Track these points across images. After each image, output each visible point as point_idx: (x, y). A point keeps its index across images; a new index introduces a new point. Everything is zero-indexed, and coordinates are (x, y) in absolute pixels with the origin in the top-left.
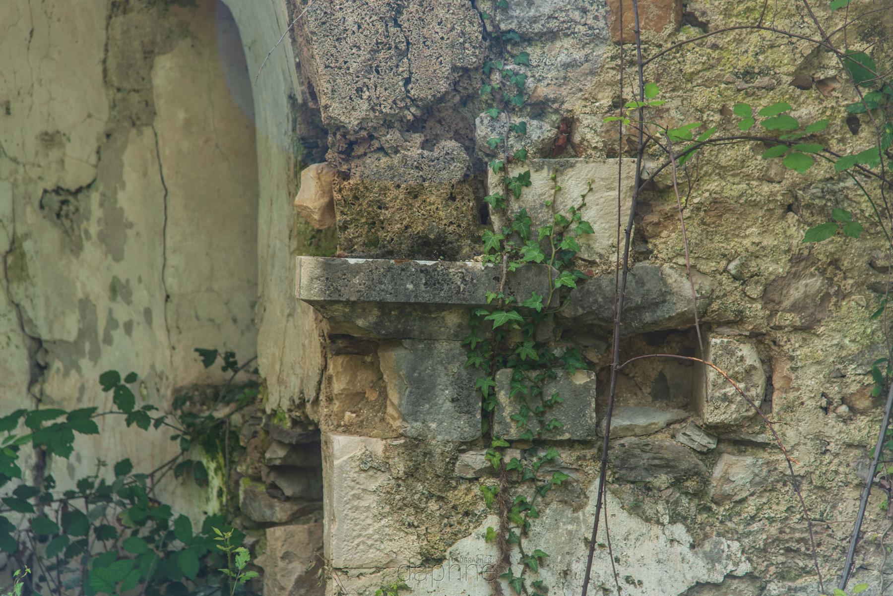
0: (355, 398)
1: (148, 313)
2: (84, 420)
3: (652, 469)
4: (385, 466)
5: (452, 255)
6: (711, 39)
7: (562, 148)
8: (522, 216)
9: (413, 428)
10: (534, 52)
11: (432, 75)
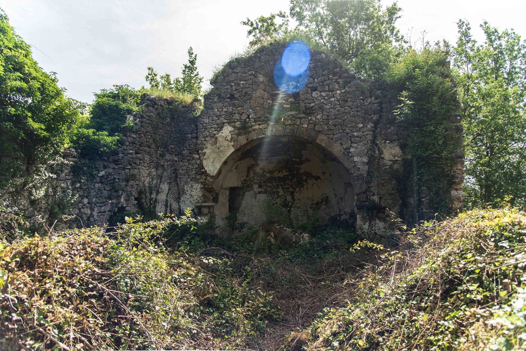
2: (342, 215)
7: (374, 195)
11: (364, 190)
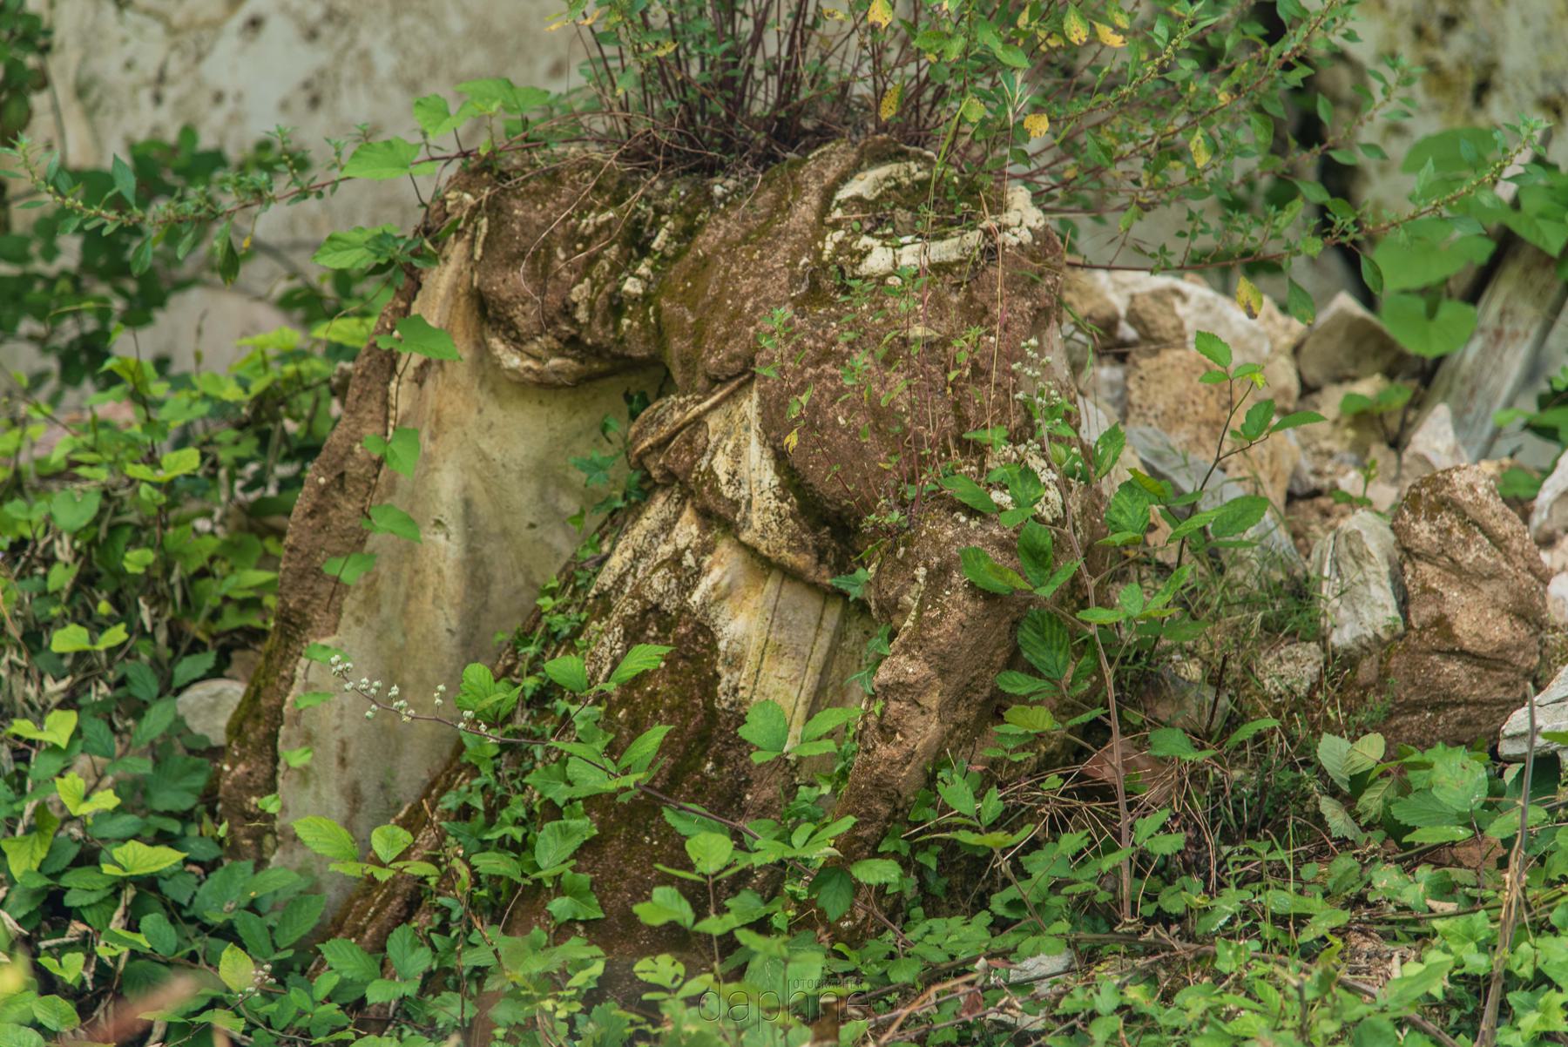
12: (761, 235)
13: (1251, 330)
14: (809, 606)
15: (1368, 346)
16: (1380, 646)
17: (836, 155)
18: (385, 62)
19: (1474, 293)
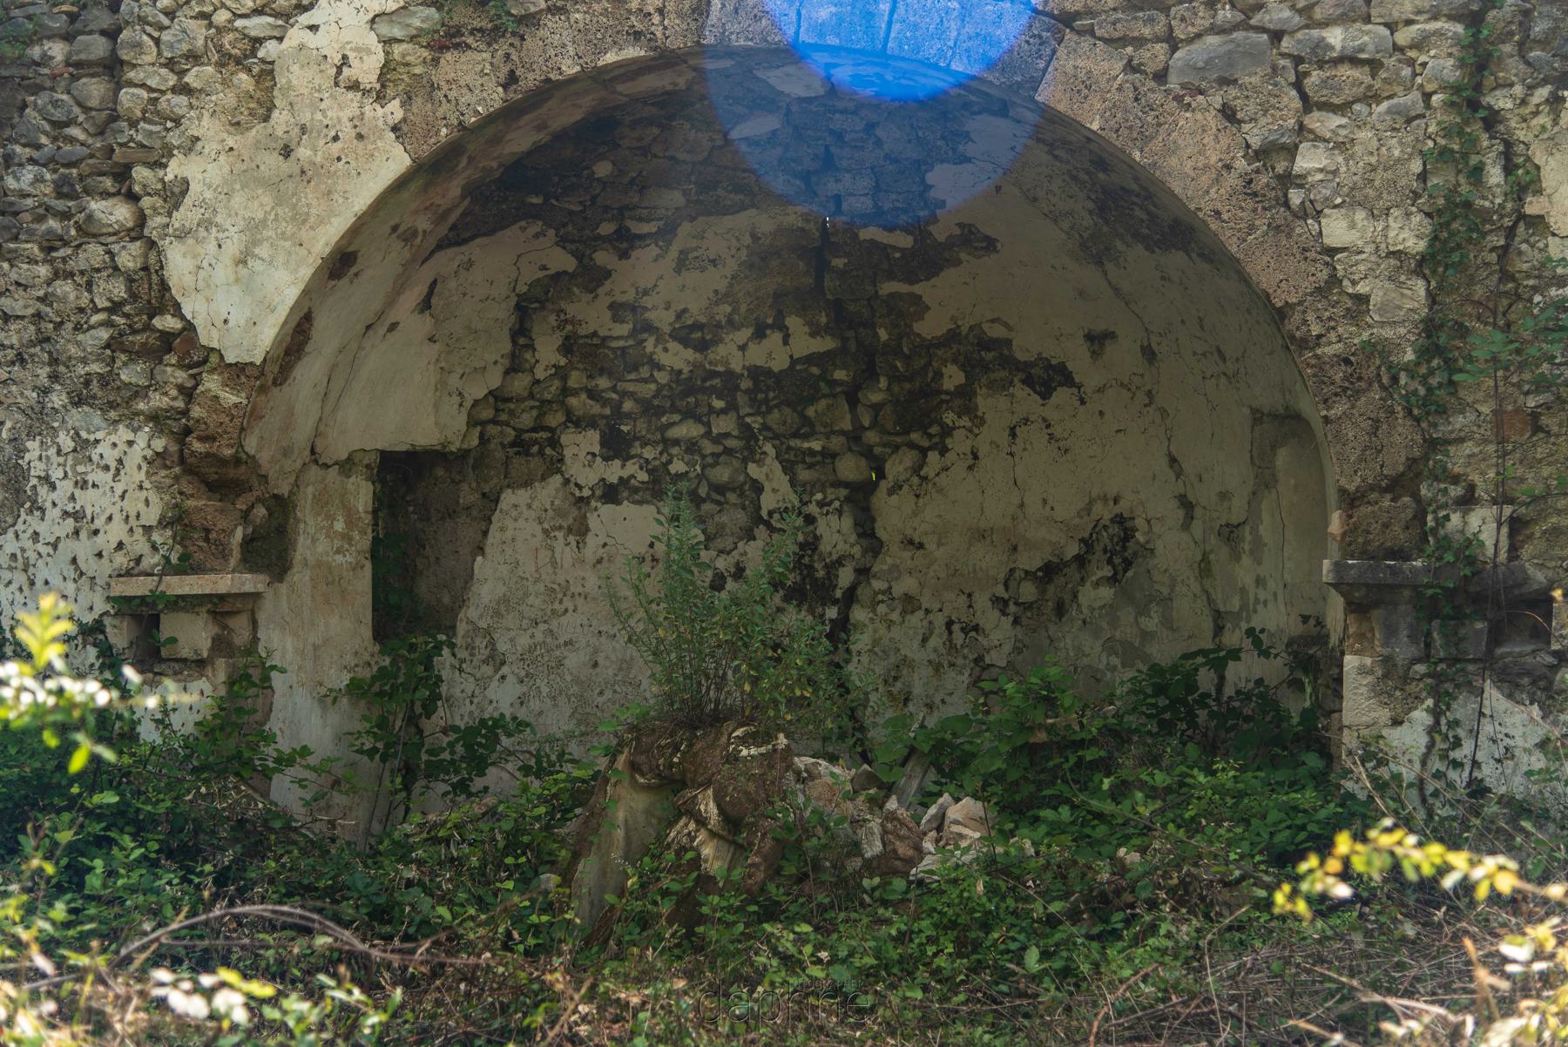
0: (1361, 637)
1: (1275, 594)
2: (1235, 654)
3: (1520, 675)
4: (1371, 672)
5: (1408, 558)
6: (1552, 439)
7: (1468, 501)
8: (1446, 537)
9: (1386, 651)
10: (1452, 449)
11: (1395, 461)
12: (712, 746)
13: (837, 774)
14: (726, 846)
15: (872, 779)
16: (877, 857)
17: (730, 725)
18: (545, 690)
19: (903, 765)
